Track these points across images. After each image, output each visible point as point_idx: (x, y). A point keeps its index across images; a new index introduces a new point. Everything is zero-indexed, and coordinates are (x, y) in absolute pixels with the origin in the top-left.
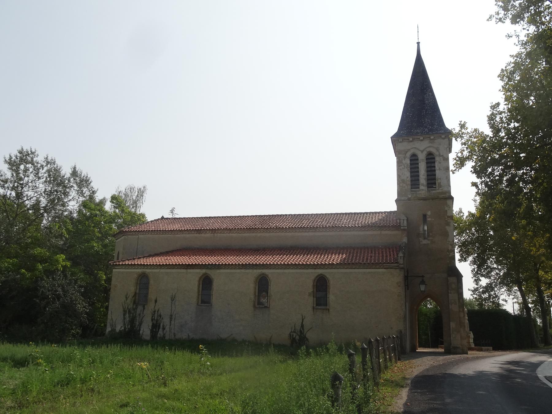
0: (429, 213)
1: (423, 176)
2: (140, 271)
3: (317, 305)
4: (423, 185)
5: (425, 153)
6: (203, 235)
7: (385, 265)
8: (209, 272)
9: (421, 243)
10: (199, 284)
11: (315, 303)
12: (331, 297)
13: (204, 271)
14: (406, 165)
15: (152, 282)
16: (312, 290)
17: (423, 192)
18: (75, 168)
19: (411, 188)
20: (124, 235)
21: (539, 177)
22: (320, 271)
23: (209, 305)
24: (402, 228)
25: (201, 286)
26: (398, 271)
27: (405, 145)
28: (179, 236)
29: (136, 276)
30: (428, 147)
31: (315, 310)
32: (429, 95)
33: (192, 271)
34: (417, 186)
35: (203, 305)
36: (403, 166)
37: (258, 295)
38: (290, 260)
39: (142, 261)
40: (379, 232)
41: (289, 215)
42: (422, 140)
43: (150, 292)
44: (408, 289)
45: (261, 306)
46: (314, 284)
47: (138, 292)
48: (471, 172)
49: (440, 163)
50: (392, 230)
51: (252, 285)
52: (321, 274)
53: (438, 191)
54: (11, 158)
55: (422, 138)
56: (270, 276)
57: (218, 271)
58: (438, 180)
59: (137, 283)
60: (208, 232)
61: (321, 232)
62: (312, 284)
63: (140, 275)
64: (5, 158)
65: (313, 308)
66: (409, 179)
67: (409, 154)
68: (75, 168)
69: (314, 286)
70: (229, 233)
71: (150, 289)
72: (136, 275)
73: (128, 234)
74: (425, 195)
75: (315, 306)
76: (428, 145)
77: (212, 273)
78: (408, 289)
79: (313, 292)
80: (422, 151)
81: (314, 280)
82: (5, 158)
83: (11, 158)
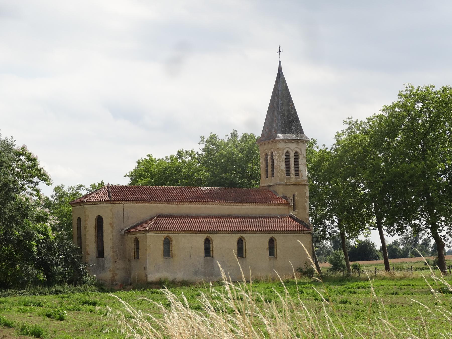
0: (296, 194)
1: (293, 168)
4: (293, 174)
5: (294, 152)
6: (170, 205)
7: (305, 231)
14: (283, 159)
15: (174, 242)
17: (293, 179)
28: (154, 205)
29: (163, 239)
30: (295, 148)
36: (282, 160)
48: (201, 137)
49: (302, 160)
50: (284, 206)
52: (272, 237)
53: (301, 179)
54: (139, 160)
56: (173, 238)
57: (216, 235)
58: (301, 172)
62: (278, 242)
66: (285, 169)
67: (285, 152)
72: (163, 238)
73: (116, 203)
74: (294, 181)
80: (292, 150)
83: (139, 160)
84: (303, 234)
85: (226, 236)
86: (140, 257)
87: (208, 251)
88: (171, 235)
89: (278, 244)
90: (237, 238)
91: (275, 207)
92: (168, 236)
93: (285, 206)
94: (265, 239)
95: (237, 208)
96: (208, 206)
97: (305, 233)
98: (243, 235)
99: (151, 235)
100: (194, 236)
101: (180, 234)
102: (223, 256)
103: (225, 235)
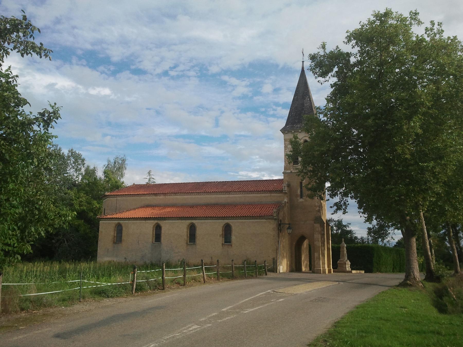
2: (117, 222)
3: (225, 242)
6: (158, 197)
7: (265, 217)
8: (159, 222)
9: (298, 201)
10: (153, 230)
11: (224, 241)
12: (233, 238)
13: (156, 221)
15: (124, 229)
16: (221, 233)
18: (456, 36)
19: (293, 164)
20: (107, 198)
21: (67, 198)
22: (226, 221)
23: (160, 243)
24: (284, 192)
25: (154, 231)
26: (273, 220)
27: (291, 136)
31: (223, 246)
32: (307, 100)
33: (148, 221)
34: (297, 163)
35: (156, 243)
36: (288, 150)
37: (116, 235)
38: (248, 212)
39: (118, 216)
40: (270, 195)
41: (217, 182)
42: (300, 132)
43: (123, 235)
44: (281, 232)
45: (191, 243)
46: (223, 229)
47: (115, 235)
50: (278, 193)
51: (185, 230)
52: (227, 223)
55: (300, 131)
56: (123, 225)
57: (165, 221)
59: (115, 230)
60: (161, 195)
61: (233, 194)
62: (221, 229)
63: (117, 225)
64: (56, 137)
65: (223, 244)
68: (456, 36)
69: (223, 230)
70: (175, 196)
71: (123, 233)
75: (224, 243)
76: (304, 136)
77: (162, 223)
78: (281, 232)
79: (223, 234)
81: (223, 226)
82: (56, 137)
84: (265, 220)
85: (175, 222)
86: (124, 238)
87: (158, 237)
88: (121, 222)
89: (233, 230)
90: (187, 224)
91: (267, 195)
92: (192, 223)
93: (280, 193)
94: (219, 225)
95: (224, 197)
96: (194, 196)
97: (267, 219)
98: (194, 221)
99: (103, 223)
100: (143, 222)
101: (130, 221)
102: (171, 242)
103: (174, 221)
